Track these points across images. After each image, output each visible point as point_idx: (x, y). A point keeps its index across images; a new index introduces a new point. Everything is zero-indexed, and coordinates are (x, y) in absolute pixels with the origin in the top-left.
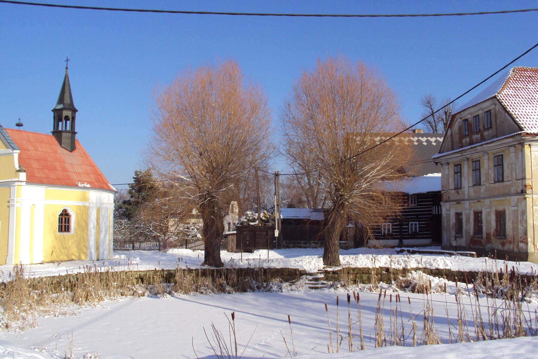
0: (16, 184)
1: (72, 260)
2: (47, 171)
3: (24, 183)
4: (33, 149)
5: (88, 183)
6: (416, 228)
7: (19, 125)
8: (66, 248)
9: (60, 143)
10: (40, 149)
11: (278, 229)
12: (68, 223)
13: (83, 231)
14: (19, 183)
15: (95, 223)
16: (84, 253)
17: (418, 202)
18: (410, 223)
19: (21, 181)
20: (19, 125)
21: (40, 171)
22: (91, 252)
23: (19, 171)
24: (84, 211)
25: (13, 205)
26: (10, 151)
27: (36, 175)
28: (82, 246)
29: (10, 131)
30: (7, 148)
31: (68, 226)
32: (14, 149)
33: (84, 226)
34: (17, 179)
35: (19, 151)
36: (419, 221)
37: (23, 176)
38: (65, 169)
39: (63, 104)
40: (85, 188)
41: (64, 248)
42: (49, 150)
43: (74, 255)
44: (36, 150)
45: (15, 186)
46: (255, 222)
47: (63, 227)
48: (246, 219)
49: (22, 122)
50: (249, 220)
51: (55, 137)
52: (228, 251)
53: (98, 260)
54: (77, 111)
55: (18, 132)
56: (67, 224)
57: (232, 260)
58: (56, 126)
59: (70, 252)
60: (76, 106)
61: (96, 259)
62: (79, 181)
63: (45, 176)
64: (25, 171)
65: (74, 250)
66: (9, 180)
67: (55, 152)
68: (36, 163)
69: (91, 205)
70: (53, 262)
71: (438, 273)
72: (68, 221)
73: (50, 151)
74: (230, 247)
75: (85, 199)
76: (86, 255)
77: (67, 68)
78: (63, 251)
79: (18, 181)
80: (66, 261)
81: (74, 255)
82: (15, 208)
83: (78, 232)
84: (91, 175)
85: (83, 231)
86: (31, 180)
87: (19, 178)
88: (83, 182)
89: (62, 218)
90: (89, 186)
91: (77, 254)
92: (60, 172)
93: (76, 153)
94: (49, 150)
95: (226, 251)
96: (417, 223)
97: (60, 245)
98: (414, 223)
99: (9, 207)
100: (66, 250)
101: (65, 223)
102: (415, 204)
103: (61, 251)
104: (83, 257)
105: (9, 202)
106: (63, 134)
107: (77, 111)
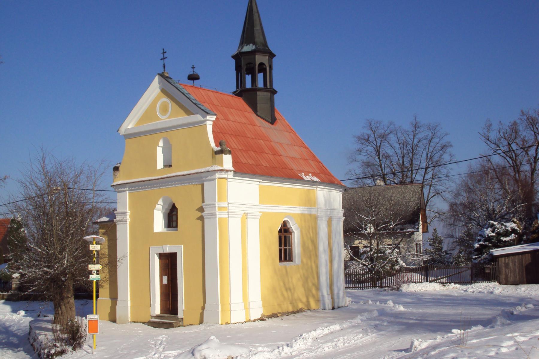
0: (218, 175)
1: (300, 311)
3: (230, 175)
4: (222, 117)
5: (314, 174)
8: (290, 290)
9: (255, 111)
12: (289, 246)
13: (310, 258)
14: (224, 175)
15: (327, 243)
16: (313, 296)
19: (227, 171)
20: (193, 77)
22: (323, 295)
23: (222, 152)
24: (311, 222)
25: (214, 214)
26: (198, 117)
28: (310, 284)
30: (189, 112)
31: (289, 249)
32: (208, 113)
33: (311, 251)
34: (219, 168)
35: (213, 118)
37: (227, 161)
39: (254, 43)
40: (312, 183)
41: (286, 290)
42: (244, 120)
43: (301, 302)
45: (214, 179)
46: (508, 236)
47: (283, 251)
48: (493, 232)
49: (197, 71)
50: (499, 234)
51: (244, 100)
52: (500, 283)
53: (333, 308)
54: (274, 56)
56: (287, 248)
57: (15, 311)
58: (240, 81)
59: (296, 296)
60: (272, 47)
61: (331, 307)
62: (302, 171)
64: (230, 152)
65: (300, 293)
66: (202, 170)
67: (253, 124)
69: (319, 213)
70: (274, 316)
73: (245, 122)
74: (503, 277)
75: (310, 202)
76: (318, 301)
78: (285, 293)
79: (222, 170)
80: (288, 314)
81: (301, 302)
82: (217, 219)
83: (305, 261)
85: (310, 258)
86: (241, 169)
87: (222, 165)
88: (307, 174)
90: (316, 179)
91: (304, 300)
93: (278, 125)
94: (244, 120)
95: (496, 283)
97: (282, 284)
99: (201, 219)
100: (289, 292)
103: (283, 295)
104: (313, 305)
105: (201, 209)
106: (258, 93)
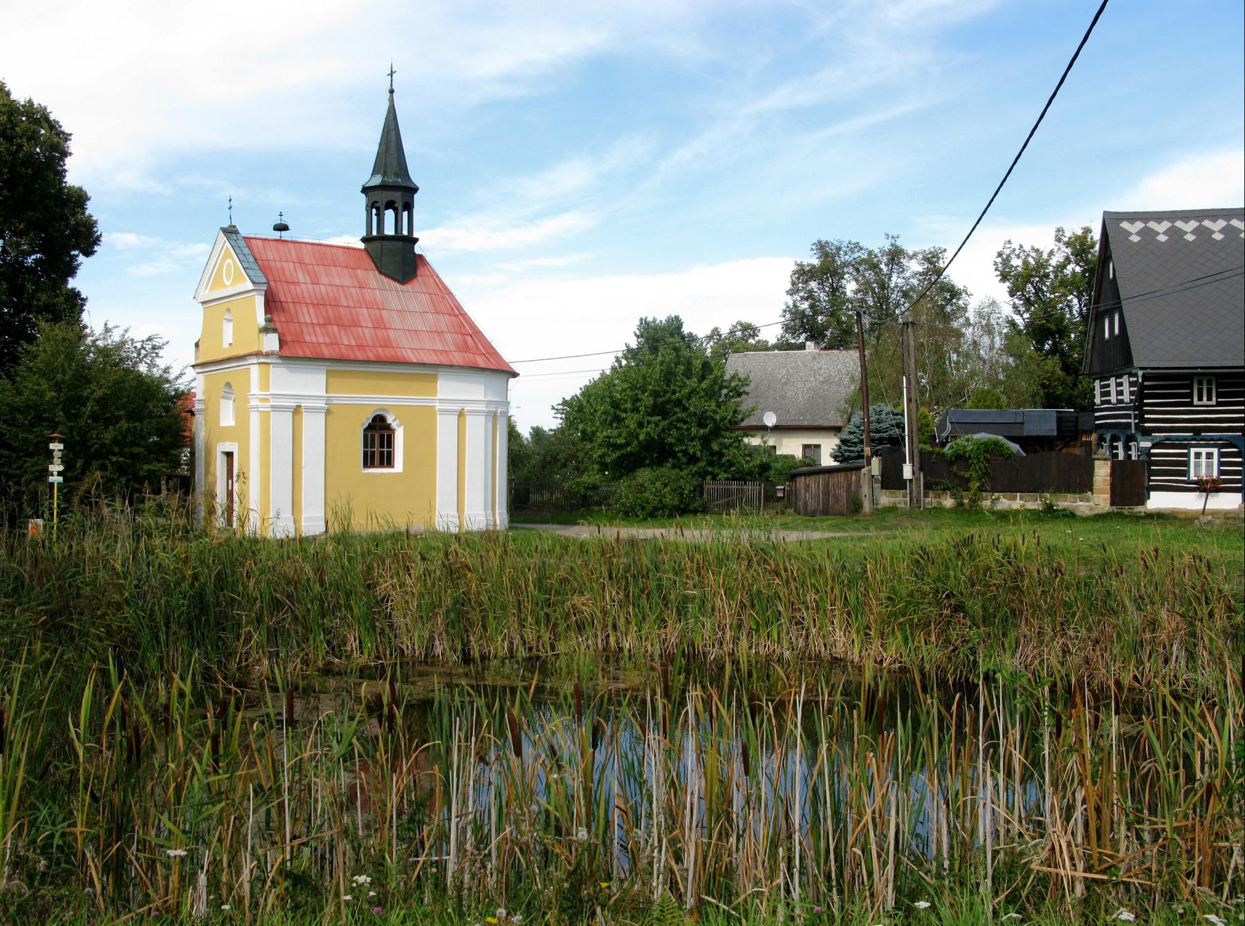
2: (335, 328)
4: (309, 280)
6: (1209, 466)
7: (282, 228)
10: (324, 280)
11: (912, 461)
17: (1219, 395)
18: (1193, 451)
20: (282, 228)
21: (318, 329)
27: (308, 339)
29: (260, 243)
36: (1220, 447)
38: (379, 324)
42: (347, 282)
44: (315, 282)
49: (286, 220)
55: (280, 245)
63: (328, 341)
68: (312, 311)
71: (338, 883)
72: (388, 441)
77: (392, 92)
84: (448, 337)
89: (373, 437)
92: (366, 331)
94: (347, 282)
96: (1215, 451)
98: (1204, 451)
101: (382, 446)
102: (1209, 399)
107: (415, 190)
